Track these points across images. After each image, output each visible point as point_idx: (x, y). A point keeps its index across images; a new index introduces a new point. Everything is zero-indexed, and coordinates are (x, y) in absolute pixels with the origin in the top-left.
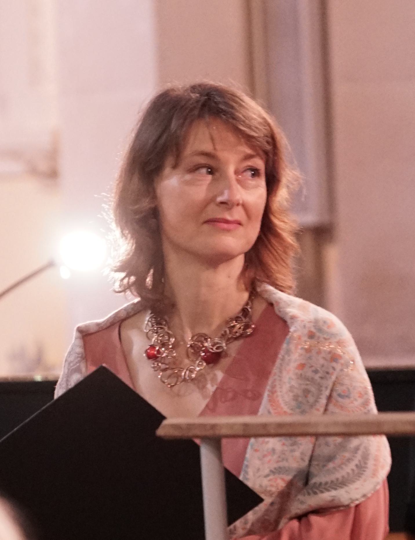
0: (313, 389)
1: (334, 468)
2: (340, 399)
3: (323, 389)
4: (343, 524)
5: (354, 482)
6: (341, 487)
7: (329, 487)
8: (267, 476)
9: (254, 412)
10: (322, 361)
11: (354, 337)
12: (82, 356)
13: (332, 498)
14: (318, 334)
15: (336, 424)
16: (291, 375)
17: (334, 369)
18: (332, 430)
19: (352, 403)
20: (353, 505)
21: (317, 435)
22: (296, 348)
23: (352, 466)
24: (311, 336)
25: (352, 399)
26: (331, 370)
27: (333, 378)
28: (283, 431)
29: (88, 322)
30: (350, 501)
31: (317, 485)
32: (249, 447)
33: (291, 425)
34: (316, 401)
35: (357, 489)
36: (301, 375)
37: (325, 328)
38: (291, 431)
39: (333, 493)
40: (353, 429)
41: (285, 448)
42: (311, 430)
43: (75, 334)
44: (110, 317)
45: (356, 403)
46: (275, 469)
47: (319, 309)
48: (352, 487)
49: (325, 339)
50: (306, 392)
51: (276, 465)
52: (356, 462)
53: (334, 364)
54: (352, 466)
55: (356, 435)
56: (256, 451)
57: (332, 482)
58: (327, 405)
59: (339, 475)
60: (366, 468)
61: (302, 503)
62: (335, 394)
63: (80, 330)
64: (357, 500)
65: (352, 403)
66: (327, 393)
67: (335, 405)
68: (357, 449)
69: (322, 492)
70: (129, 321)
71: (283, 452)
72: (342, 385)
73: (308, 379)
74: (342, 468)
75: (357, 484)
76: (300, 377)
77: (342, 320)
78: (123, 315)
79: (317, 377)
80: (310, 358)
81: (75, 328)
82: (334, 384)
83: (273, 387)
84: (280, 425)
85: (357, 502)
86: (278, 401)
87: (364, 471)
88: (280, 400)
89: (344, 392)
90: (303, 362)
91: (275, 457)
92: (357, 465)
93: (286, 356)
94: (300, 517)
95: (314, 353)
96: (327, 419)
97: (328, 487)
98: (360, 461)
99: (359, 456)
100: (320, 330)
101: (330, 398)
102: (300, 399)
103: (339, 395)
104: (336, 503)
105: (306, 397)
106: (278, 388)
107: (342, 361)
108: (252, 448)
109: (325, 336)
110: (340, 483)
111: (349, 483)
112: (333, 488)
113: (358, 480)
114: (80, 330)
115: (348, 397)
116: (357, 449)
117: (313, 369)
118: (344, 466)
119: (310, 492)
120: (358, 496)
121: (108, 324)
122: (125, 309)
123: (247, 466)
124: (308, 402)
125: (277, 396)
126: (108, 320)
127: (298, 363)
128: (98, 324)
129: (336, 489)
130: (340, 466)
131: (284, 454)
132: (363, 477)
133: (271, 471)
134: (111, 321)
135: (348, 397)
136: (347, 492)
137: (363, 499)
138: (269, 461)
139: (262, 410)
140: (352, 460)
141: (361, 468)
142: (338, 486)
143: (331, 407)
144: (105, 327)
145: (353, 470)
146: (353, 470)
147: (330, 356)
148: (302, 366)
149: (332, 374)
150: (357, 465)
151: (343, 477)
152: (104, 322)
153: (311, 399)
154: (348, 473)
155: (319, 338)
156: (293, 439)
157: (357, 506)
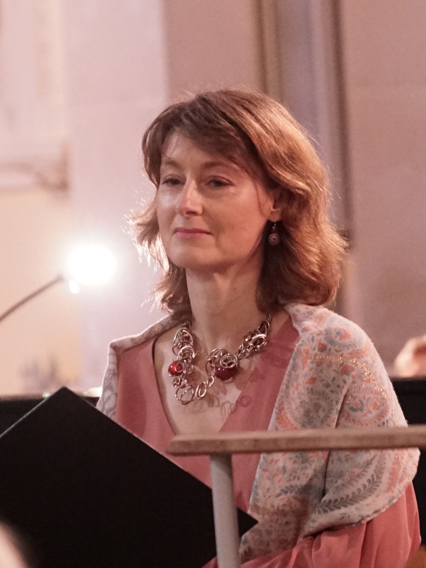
0: (323, 403)
1: (343, 485)
2: (352, 413)
3: (334, 403)
4: (350, 545)
5: (365, 498)
6: (352, 504)
7: (339, 504)
8: (278, 495)
9: (265, 428)
10: (333, 374)
11: (375, 345)
12: (114, 372)
13: (342, 516)
14: (329, 346)
15: (347, 438)
16: (302, 389)
17: (345, 382)
18: (344, 444)
19: (365, 415)
20: (364, 522)
21: (330, 450)
22: (304, 362)
23: (364, 481)
24: (323, 348)
25: (365, 412)
26: (342, 384)
27: (344, 391)
28: (296, 445)
29: (124, 338)
30: (360, 518)
31: (357, 493)
32: (259, 467)
33: (302, 439)
34: (327, 416)
35: (368, 505)
36: (312, 389)
37: (337, 339)
38: (302, 445)
39: (343, 510)
40: (365, 443)
41: (296, 466)
42: (323, 444)
43: (109, 350)
44: (146, 331)
45: (370, 416)
46: (287, 488)
47: (341, 318)
48: (363, 503)
49: (336, 351)
50: (317, 407)
51: (288, 485)
52: (368, 476)
53: (345, 377)
54: (364, 481)
55: (367, 449)
56: (265, 470)
57: (342, 499)
58: (338, 419)
59: (349, 491)
60: (380, 482)
61: (314, 521)
62: (346, 408)
63: (115, 348)
64: (368, 516)
65: (365, 415)
66: (339, 407)
67: (347, 419)
68: (368, 463)
69: (332, 510)
70: (165, 335)
71: (294, 471)
72: (354, 398)
73: (319, 394)
74: (352, 485)
75: (369, 500)
76: (311, 391)
77: (363, 328)
78: (158, 330)
79: (327, 391)
80: (321, 371)
81: (109, 345)
82: (346, 397)
83: (282, 404)
84: (292, 440)
85: (369, 519)
86: (287, 418)
87: (378, 486)
88: (289, 416)
89: (356, 405)
90: (315, 376)
91: (287, 475)
92: (369, 481)
93: (293, 373)
94: (316, 535)
95: (325, 366)
96: (340, 432)
97: (349, 500)
98: (372, 475)
99: (371, 470)
100: (332, 342)
101: (341, 412)
102: (311, 414)
103: (352, 409)
104: (348, 521)
105: (317, 412)
106: (286, 406)
107: (354, 373)
108: (261, 468)
109: (337, 348)
110: (351, 500)
111: (361, 500)
112: (343, 505)
113: (370, 495)
114: (115, 348)
115: (361, 410)
116: (368, 463)
117: (325, 382)
118: (353, 482)
119: (321, 510)
120: (370, 513)
121: (143, 340)
122: (160, 324)
123: (256, 487)
124: (319, 417)
125: (285, 413)
126: (143, 335)
127: (309, 377)
128: (132, 340)
129: (346, 506)
130: (349, 482)
131: (296, 472)
132: (376, 493)
133: (282, 490)
134: (145, 335)
135: (361, 410)
136: (356, 509)
137: (375, 515)
138: (279, 481)
139: (270, 427)
140: (364, 475)
141: (374, 483)
142: (348, 503)
143: (342, 420)
144: (140, 342)
145: (365, 486)
146: (365, 486)
147: (341, 368)
148: (313, 380)
149: (343, 387)
150: (369, 481)
151: (353, 493)
152: (139, 337)
153: (321, 414)
154: (359, 490)
155: (330, 350)
156: (304, 454)
157: (368, 523)
